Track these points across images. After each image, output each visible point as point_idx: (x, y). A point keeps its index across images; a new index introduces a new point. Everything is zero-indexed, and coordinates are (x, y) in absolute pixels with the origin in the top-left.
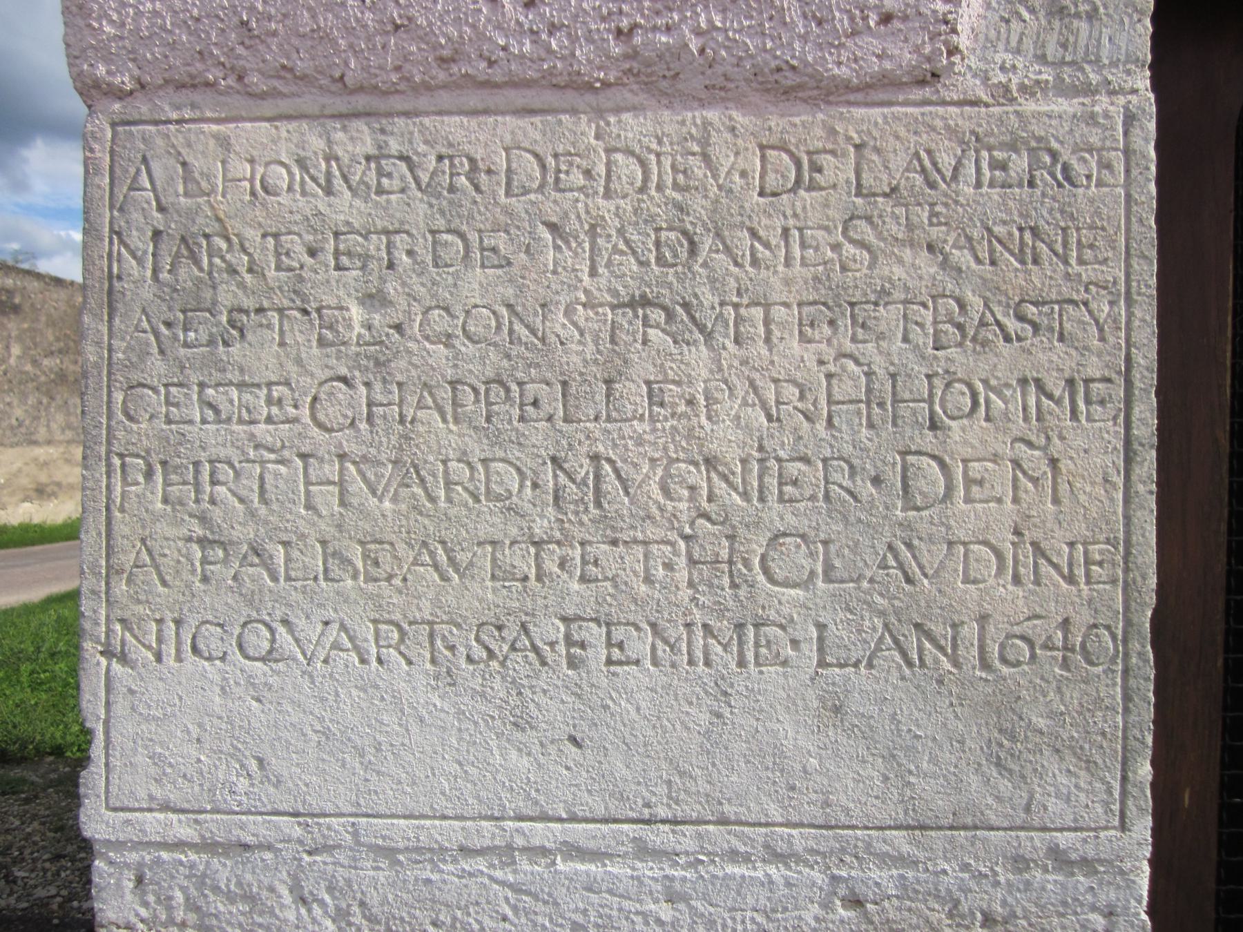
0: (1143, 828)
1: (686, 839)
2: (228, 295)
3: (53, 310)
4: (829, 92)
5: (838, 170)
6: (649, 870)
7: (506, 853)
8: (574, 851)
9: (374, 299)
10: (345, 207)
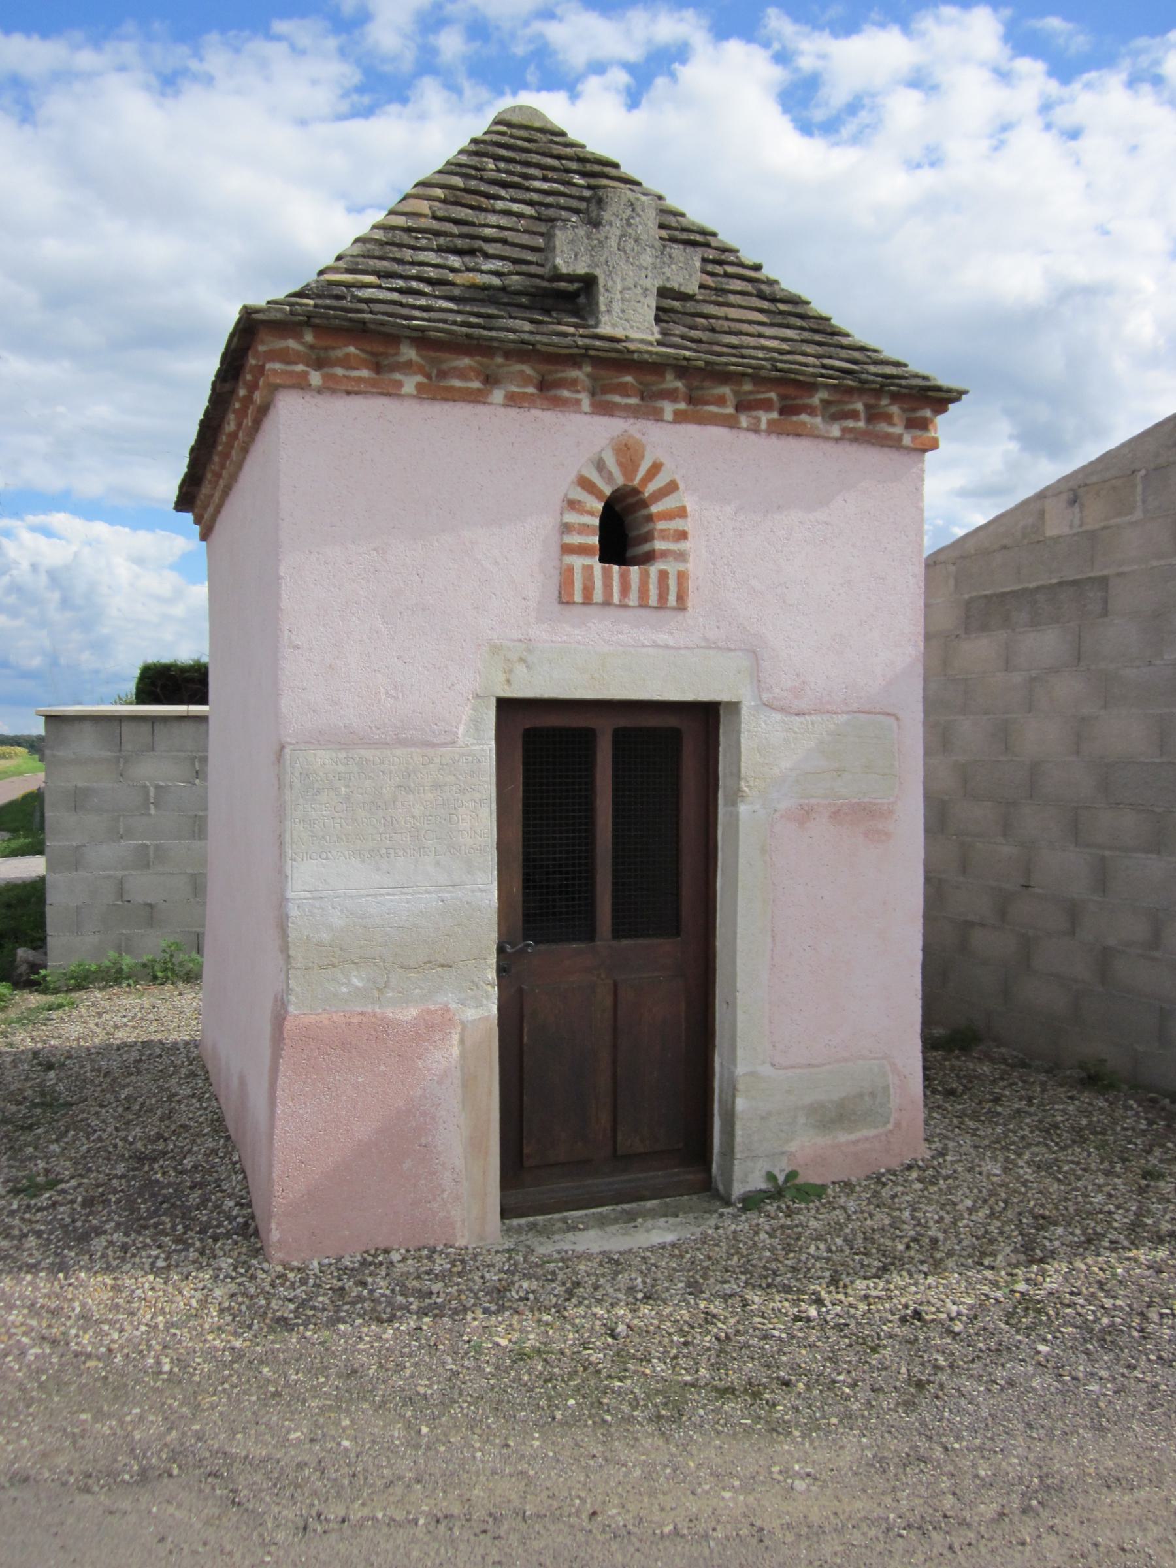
0: (495, 884)
1: (410, 890)
2: (316, 785)
3: (603, 976)
4: (435, 745)
5: (437, 760)
6: (403, 897)
7: (375, 895)
8: (389, 894)
9: (347, 786)
10: (341, 768)
